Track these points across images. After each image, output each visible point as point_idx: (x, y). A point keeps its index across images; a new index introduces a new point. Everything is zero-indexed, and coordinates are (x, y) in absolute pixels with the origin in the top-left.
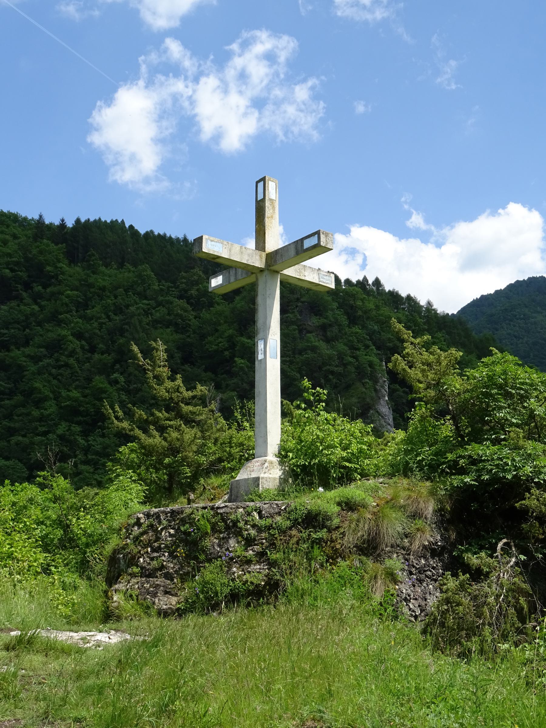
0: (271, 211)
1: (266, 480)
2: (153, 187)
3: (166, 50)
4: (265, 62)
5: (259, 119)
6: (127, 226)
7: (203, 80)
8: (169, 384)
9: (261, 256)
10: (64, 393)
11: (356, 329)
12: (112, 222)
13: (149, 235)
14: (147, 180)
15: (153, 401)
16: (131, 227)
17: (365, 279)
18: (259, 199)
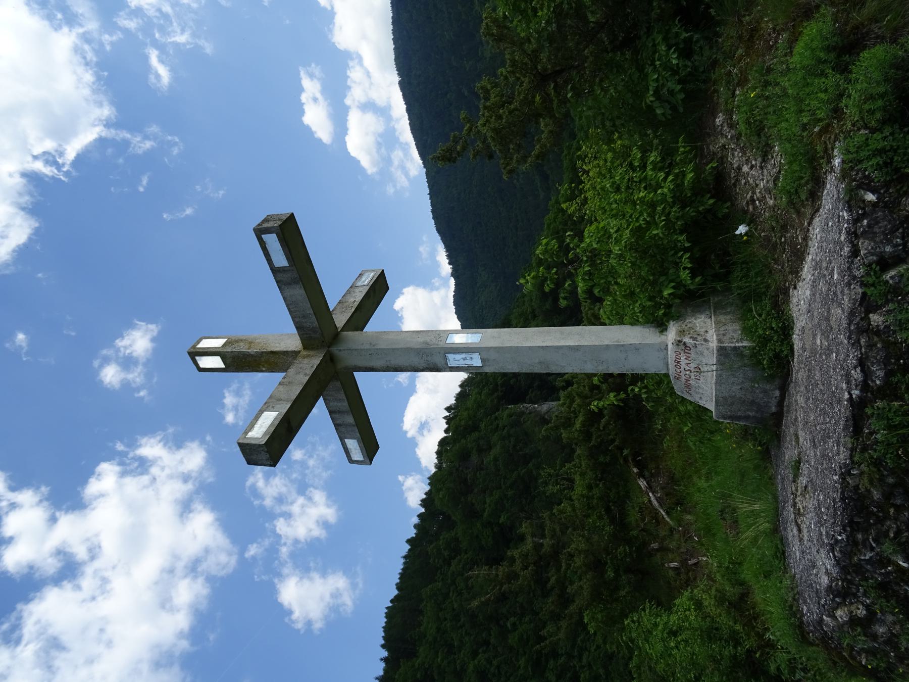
0: (242, 344)
1: (724, 335)
2: (360, 581)
3: (254, 558)
4: (271, 480)
5: (316, 488)
6: (390, 605)
7: (278, 531)
8: (518, 566)
9: (304, 357)
10: (521, 672)
11: (482, 426)
12: (386, 617)
13: (399, 587)
14: (354, 586)
15: (532, 595)
16: (392, 601)
17: (445, 418)
18: (222, 365)
